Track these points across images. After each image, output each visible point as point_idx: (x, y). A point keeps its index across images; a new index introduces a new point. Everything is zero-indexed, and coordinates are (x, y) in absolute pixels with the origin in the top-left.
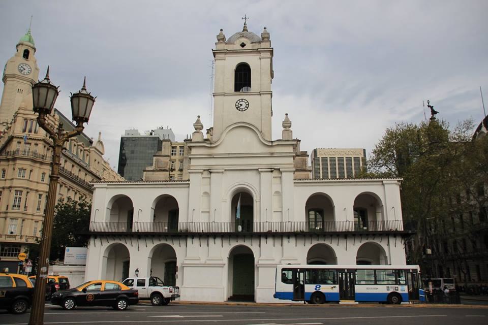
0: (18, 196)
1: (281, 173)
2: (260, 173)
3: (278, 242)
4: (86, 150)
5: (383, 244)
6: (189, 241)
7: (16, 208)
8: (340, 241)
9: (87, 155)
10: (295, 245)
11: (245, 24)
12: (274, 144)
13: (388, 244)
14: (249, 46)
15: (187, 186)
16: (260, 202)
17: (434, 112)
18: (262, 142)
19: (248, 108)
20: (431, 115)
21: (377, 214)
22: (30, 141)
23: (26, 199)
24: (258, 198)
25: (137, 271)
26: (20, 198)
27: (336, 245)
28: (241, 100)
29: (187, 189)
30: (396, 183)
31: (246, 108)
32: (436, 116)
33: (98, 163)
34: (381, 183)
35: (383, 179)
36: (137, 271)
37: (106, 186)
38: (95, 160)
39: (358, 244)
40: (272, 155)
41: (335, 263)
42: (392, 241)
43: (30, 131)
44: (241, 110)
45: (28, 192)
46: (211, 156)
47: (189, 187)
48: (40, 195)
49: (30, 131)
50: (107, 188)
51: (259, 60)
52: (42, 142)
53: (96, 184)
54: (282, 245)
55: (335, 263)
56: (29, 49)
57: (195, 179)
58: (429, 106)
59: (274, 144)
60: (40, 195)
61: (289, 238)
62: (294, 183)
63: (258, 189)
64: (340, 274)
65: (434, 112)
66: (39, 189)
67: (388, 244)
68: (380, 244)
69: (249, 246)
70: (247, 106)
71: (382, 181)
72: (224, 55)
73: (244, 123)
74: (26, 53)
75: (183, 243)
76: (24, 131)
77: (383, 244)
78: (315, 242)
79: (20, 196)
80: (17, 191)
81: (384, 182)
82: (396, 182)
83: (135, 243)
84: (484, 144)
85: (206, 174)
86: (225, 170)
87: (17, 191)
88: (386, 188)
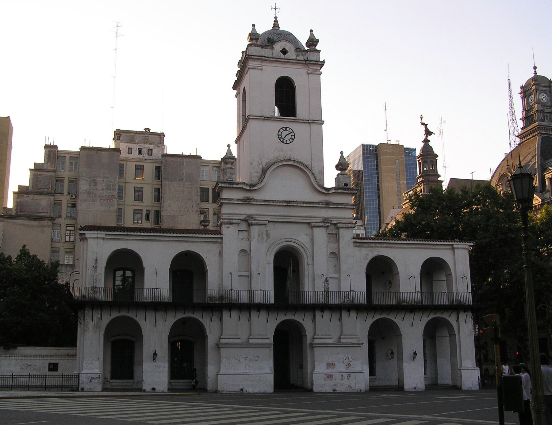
1: (338, 228)
2: (312, 227)
3: (244, 316)
5: (452, 319)
6: (226, 315)
8: (241, 313)
10: (265, 320)
11: (276, 18)
12: (330, 192)
13: (458, 320)
14: (292, 55)
15: (219, 240)
16: (313, 264)
17: (428, 133)
18: (313, 185)
19: (293, 139)
20: (425, 137)
21: (434, 282)
24: (310, 260)
25: (155, 354)
27: (208, 321)
28: (284, 129)
29: (218, 245)
30: (467, 249)
32: (429, 138)
34: (450, 247)
35: (453, 243)
36: (155, 354)
37: (103, 236)
39: (172, 319)
40: (327, 205)
42: (462, 316)
47: (60, 226)
50: (104, 239)
51: (307, 76)
54: (249, 319)
57: (228, 232)
58: (423, 124)
59: (330, 192)
61: (349, 311)
62: (354, 242)
63: (310, 250)
65: (428, 133)
67: (458, 320)
68: (394, 320)
69: (300, 321)
70: (293, 137)
71: (452, 245)
72: (260, 63)
75: (216, 319)
77: (452, 319)
78: (432, 316)
81: (455, 246)
82: (467, 247)
83: (151, 315)
85: (244, 226)
86: (269, 222)
88: (455, 252)
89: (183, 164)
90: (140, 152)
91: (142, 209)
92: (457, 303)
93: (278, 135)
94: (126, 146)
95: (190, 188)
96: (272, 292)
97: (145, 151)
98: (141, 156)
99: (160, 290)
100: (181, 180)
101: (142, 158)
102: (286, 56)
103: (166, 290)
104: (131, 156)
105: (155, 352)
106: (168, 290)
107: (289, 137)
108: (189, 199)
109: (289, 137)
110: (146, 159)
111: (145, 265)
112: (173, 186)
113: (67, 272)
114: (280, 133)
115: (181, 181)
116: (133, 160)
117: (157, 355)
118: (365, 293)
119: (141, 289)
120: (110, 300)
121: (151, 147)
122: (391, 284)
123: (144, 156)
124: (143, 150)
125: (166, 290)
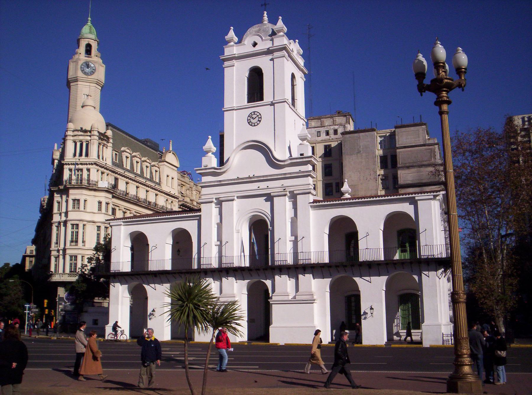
0: (75, 230)
4: (154, 166)
7: (74, 244)
9: (156, 171)
22: (80, 167)
23: (83, 232)
26: (77, 232)
31: (258, 122)
33: (172, 178)
38: (168, 176)
41: (272, 299)
43: (81, 155)
44: (253, 125)
45: (84, 225)
46: (221, 184)
48: (99, 227)
49: (81, 155)
52: (94, 166)
53: (417, 195)
55: (272, 299)
56: (90, 43)
60: (99, 227)
64: (53, 311)
66: (96, 219)
70: (249, 121)
73: (248, 142)
74: (88, 48)
76: (75, 155)
79: (77, 230)
80: (73, 225)
84: (504, 147)
87: (73, 225)
89: (359, 138)
90: (327, 133)
91: (83, 200)
92: (448, 256)
93: (248, 120)
94: (315, 131)
95: (367, 158)
96: (248, 256)
97: (331, 132)
98: (328, 137)
99: (429, 246)
100: (359, 152)
101: (329, 138)
102: (257, 48)
103: (443, 246)
104: (320, 139)
105: (371, 307)
106: (445, 245)
107: (254, 116)
108: (367, 169)
109: (254, 116)
110: (332, 139)
111: (150, 243)
112: (352, 159)
113: (486, 229)
114: (256, 124)
115: (359, 154)
116: (322, 141)
117: (373, 309)
118: (328, 252)
119: (378, 249)
120: (326, 262)
121: (336, 127)
122: (180, 250)
123: (330, 137)
124: (330, 131)
125: (443, 246)
